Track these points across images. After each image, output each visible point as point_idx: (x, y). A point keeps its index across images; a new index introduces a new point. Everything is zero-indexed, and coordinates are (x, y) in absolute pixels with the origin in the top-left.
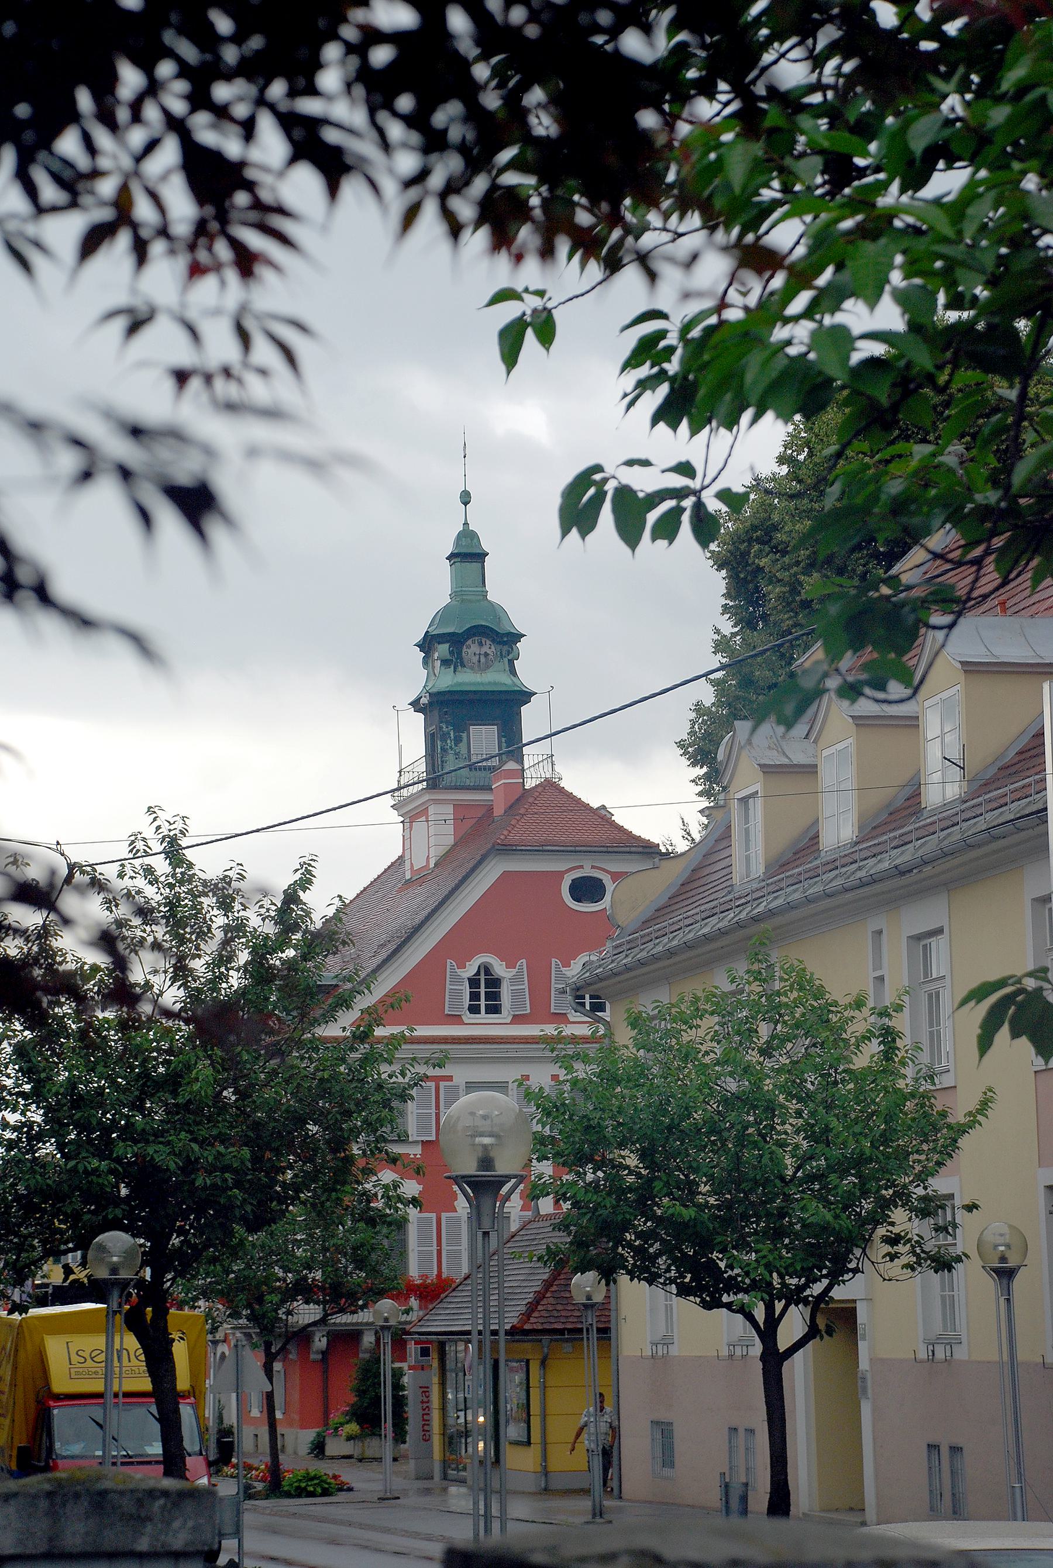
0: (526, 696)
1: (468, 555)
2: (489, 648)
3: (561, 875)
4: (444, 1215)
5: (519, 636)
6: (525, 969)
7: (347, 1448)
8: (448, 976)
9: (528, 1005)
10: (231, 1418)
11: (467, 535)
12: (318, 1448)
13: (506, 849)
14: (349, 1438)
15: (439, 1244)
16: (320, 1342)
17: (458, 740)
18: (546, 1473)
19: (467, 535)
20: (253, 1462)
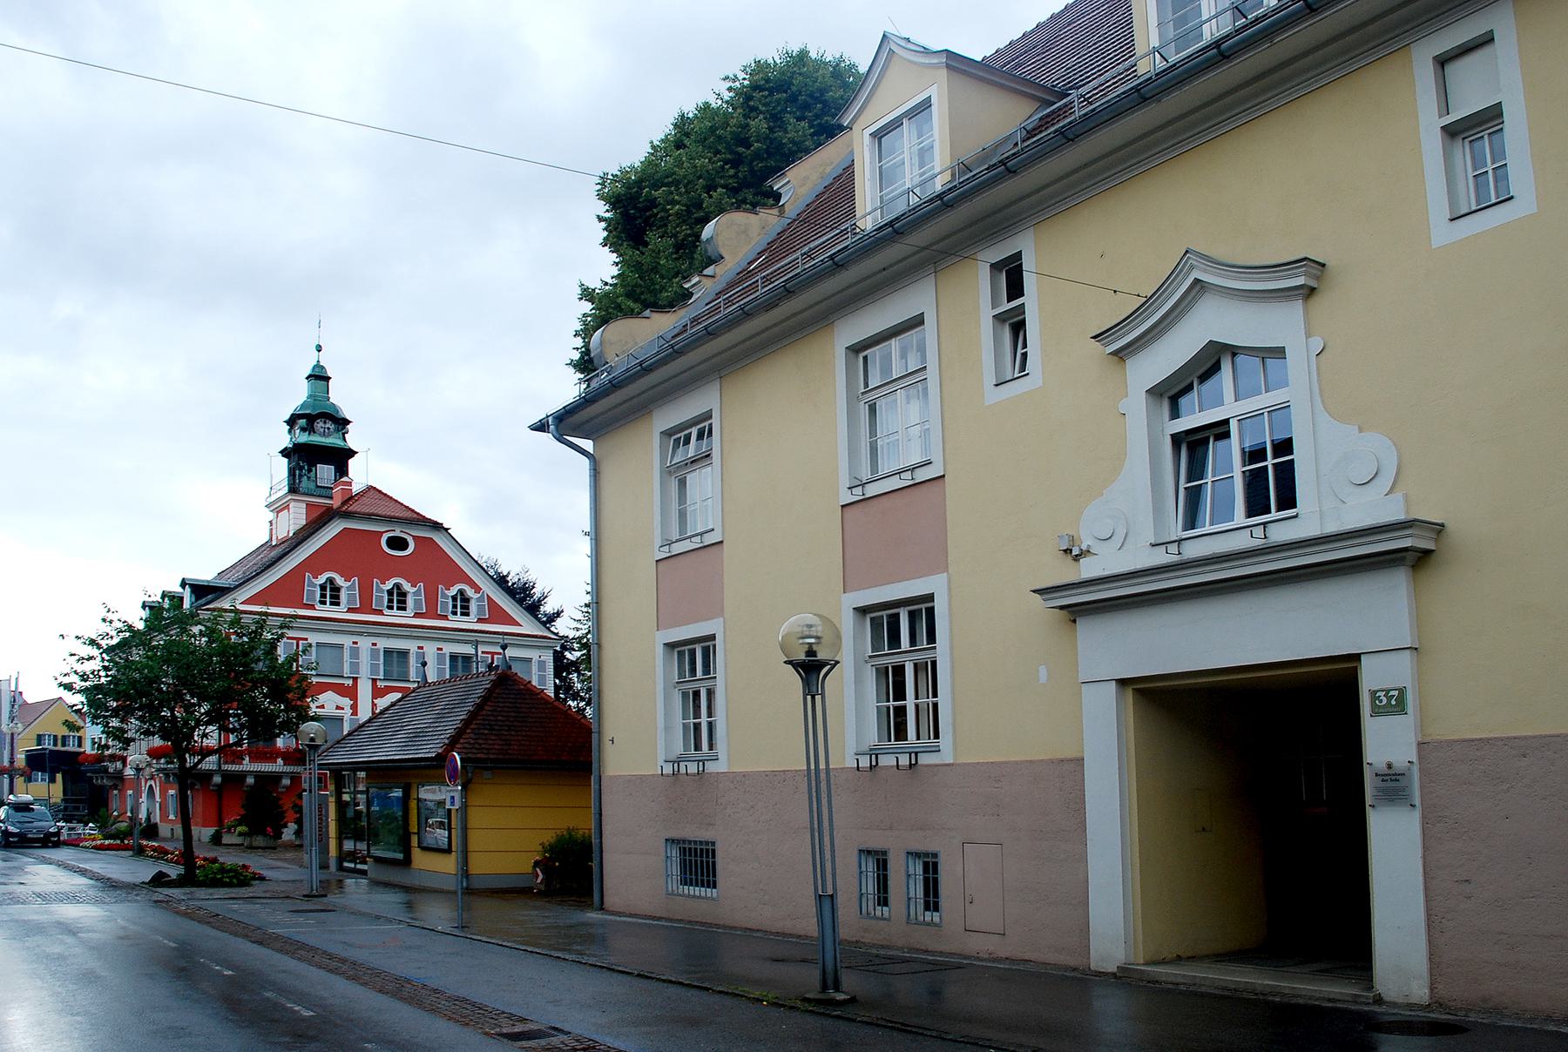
0: (352, 453)
1: (319, 377)
2: (329, 425)
5: (348, 422)
7: (238, 840)
10: (157, 818)
11: (318, 366)
12: (216, 840)
13: (348, 515)
14: (240, 834)
16: (217, 779)
17: (310, 471)
18: (465, 873)
19: (318, 366)
20: (169, 846)
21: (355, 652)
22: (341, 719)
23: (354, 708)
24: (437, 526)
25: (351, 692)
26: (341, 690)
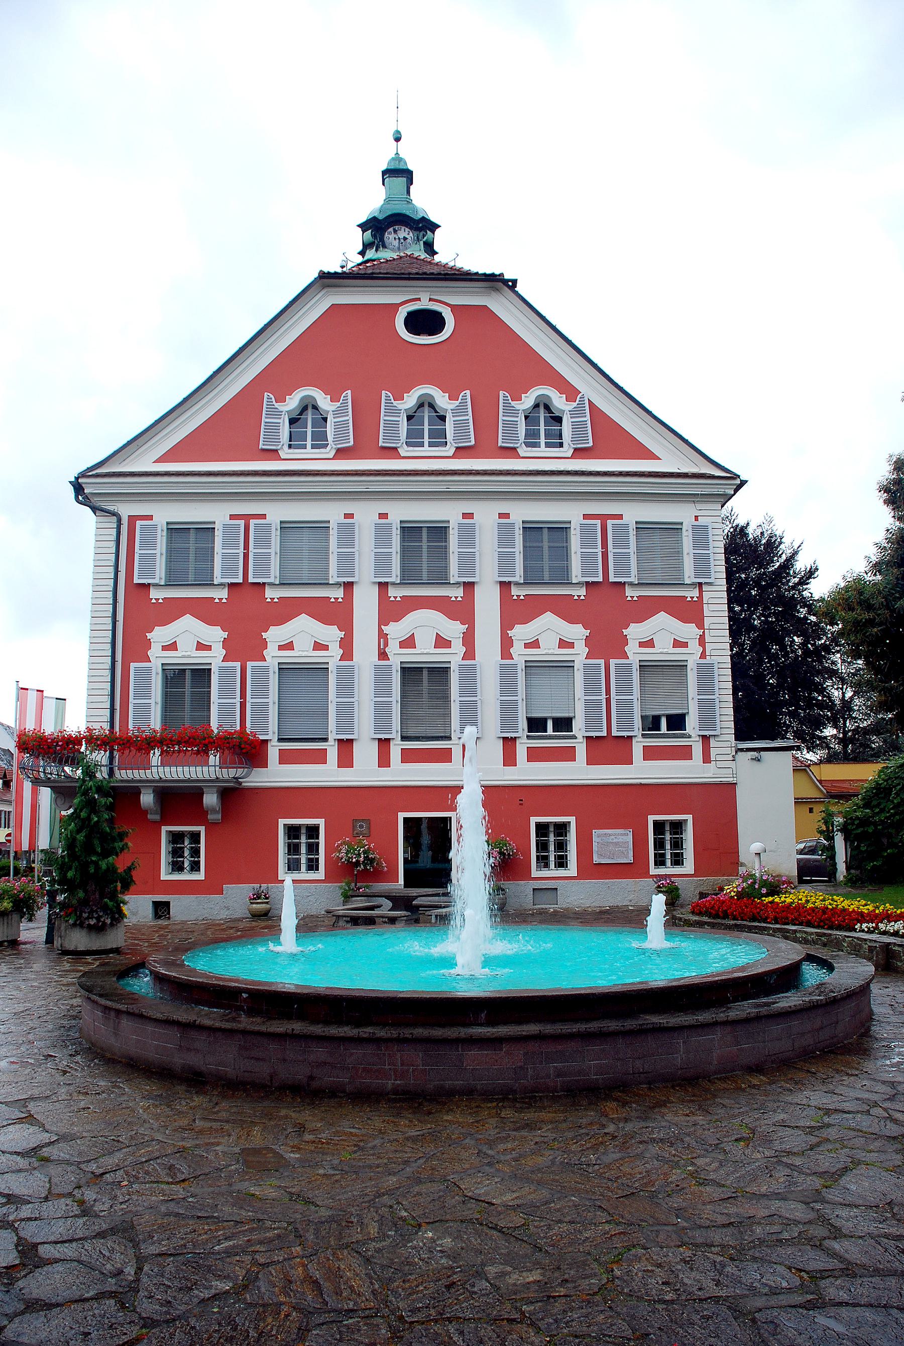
1: (398, 174)
3: (395, 307)
4: (613, 662)
5: (433, 227)
6: (469, 400)
8: (383, 407)
9: (590, 438)
11: (397, 158)
15: (608, 692)
19: (397, 158)
21: (348, 533)
22: (323, 670)
23: (347, 646)
24: (495, 282)
25: (338, 614)
26: (324, 612)
